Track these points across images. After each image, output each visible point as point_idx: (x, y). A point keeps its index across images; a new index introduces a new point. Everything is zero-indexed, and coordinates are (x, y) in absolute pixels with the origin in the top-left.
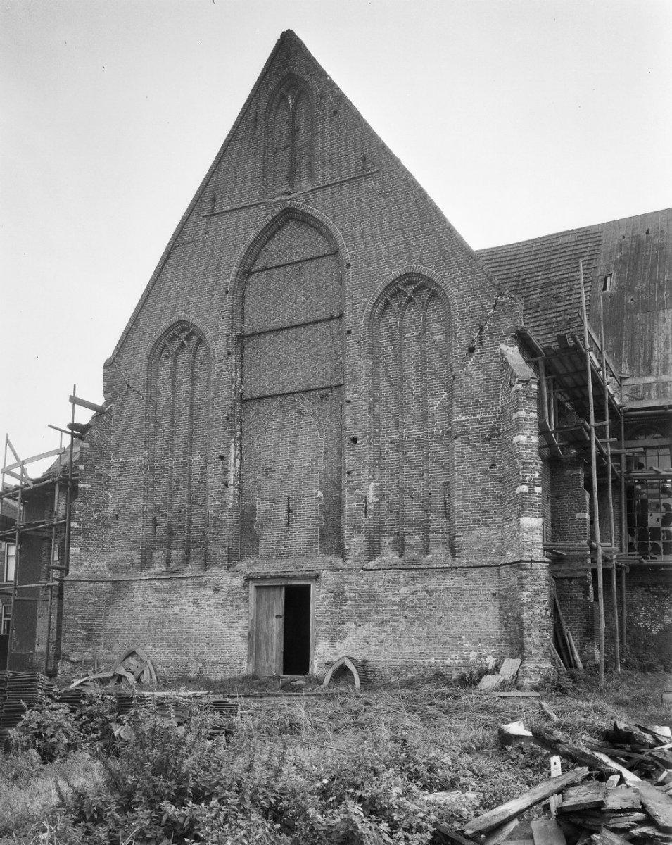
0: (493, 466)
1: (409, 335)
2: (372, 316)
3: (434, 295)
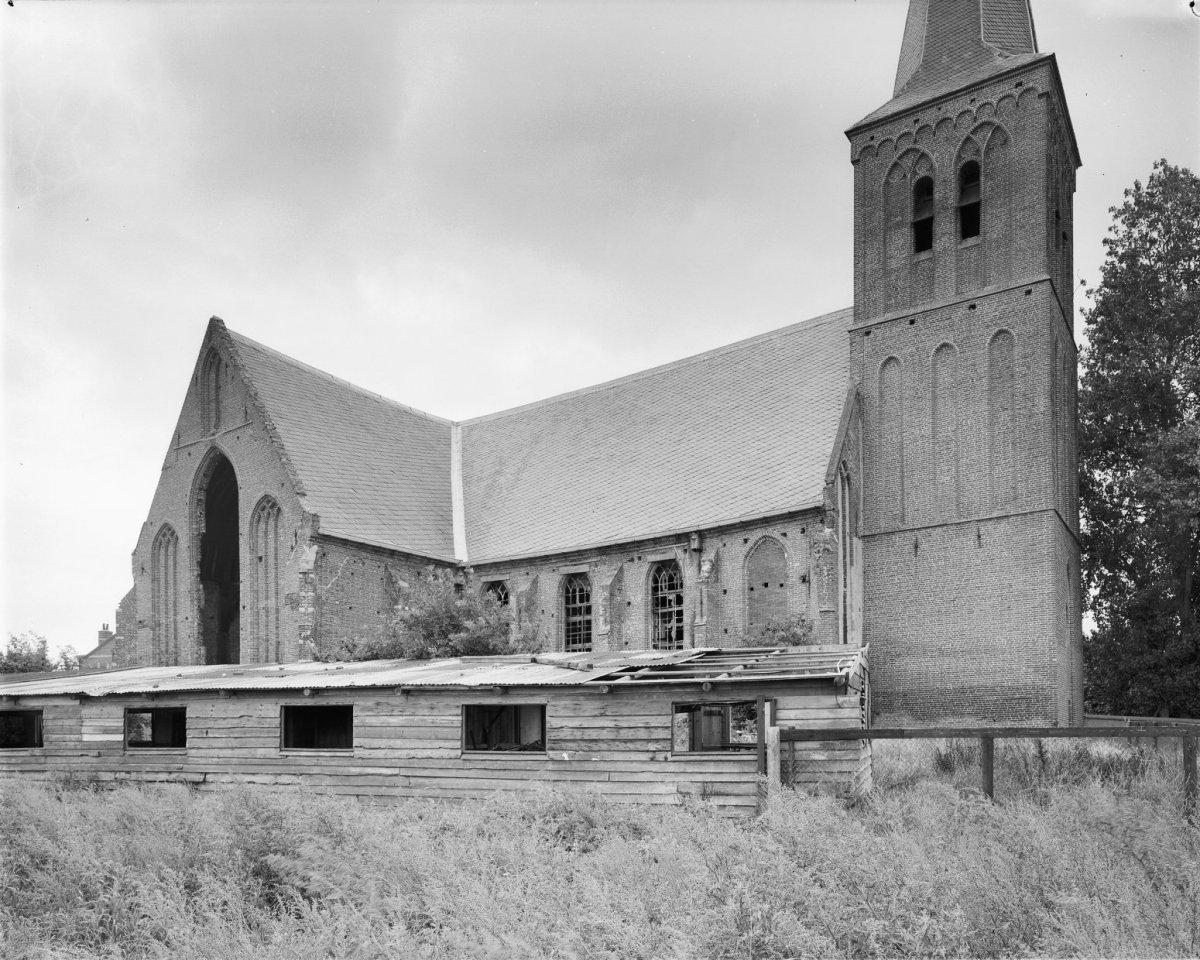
2: (251, 524)
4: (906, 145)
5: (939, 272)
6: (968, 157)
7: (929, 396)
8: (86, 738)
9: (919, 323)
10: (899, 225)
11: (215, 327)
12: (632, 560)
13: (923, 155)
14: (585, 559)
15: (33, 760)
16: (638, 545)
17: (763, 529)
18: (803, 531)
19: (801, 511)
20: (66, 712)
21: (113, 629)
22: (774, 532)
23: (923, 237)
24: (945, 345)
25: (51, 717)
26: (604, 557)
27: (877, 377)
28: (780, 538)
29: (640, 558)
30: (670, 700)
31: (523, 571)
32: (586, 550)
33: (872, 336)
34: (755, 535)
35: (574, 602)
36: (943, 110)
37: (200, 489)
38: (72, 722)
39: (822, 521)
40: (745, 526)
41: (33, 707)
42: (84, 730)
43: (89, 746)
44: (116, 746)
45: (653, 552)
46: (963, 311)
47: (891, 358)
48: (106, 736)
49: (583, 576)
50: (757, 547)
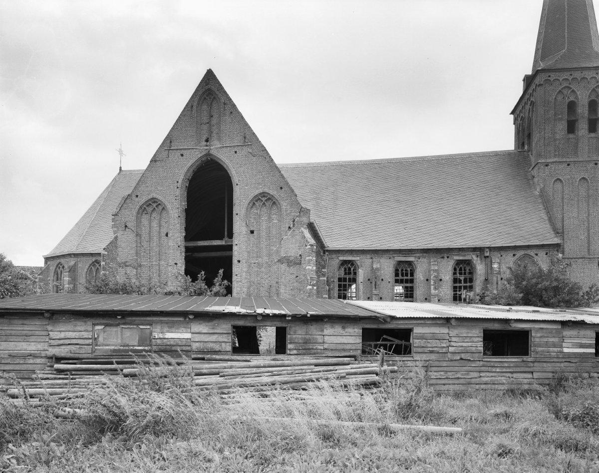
0: (297, 277)
2: (247, 209)
3: (274, 203)
4: (565, 84)
5: (580, 145)
6: (593, 97)
7: (576, 199)
8: (566, 350)
9: (572, 165)
10: (561, 119)
11: (210, 76)
12: (443, 258)
13: (573, 91)
14: (412, 254)
15: (522, 364)
16: (449, 251)
17: (525, 251)
18: (546, 254)
19: (548, 244)
20: (551, 333)
21: (5, 260)
22: (532, 253)
23: (571, 127)
24: (583, 178)
25: (539, 335)
26: (425, 254)
27: (551, 186)
28: (534, 256)
29: (448, 257)
30: (361, 327)
31: (369, 256)
32: (415, 249)
33: (549, 167)
34: (520, 253)
35: (407, 276)
36: (584, 73)
38: (556, 340)
39: (557, 251)
40: (516, 248)
41: (523, 328)
42: (564, 345)
43: (570, 355)
44: (590, 356)
45: (457, 255)
46: (592, 165)
47: (558, 179)
48: (582, 349)
49: (410, 263)
50: (520, 259)
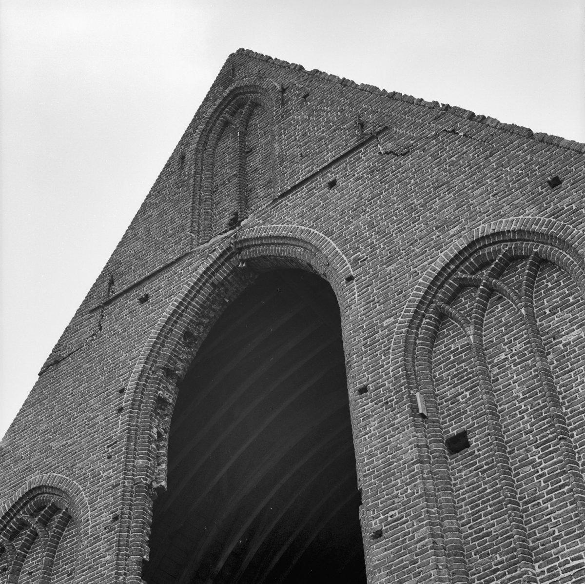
1: (503, 356)
3: (542, 263)
37: (169, 372)
